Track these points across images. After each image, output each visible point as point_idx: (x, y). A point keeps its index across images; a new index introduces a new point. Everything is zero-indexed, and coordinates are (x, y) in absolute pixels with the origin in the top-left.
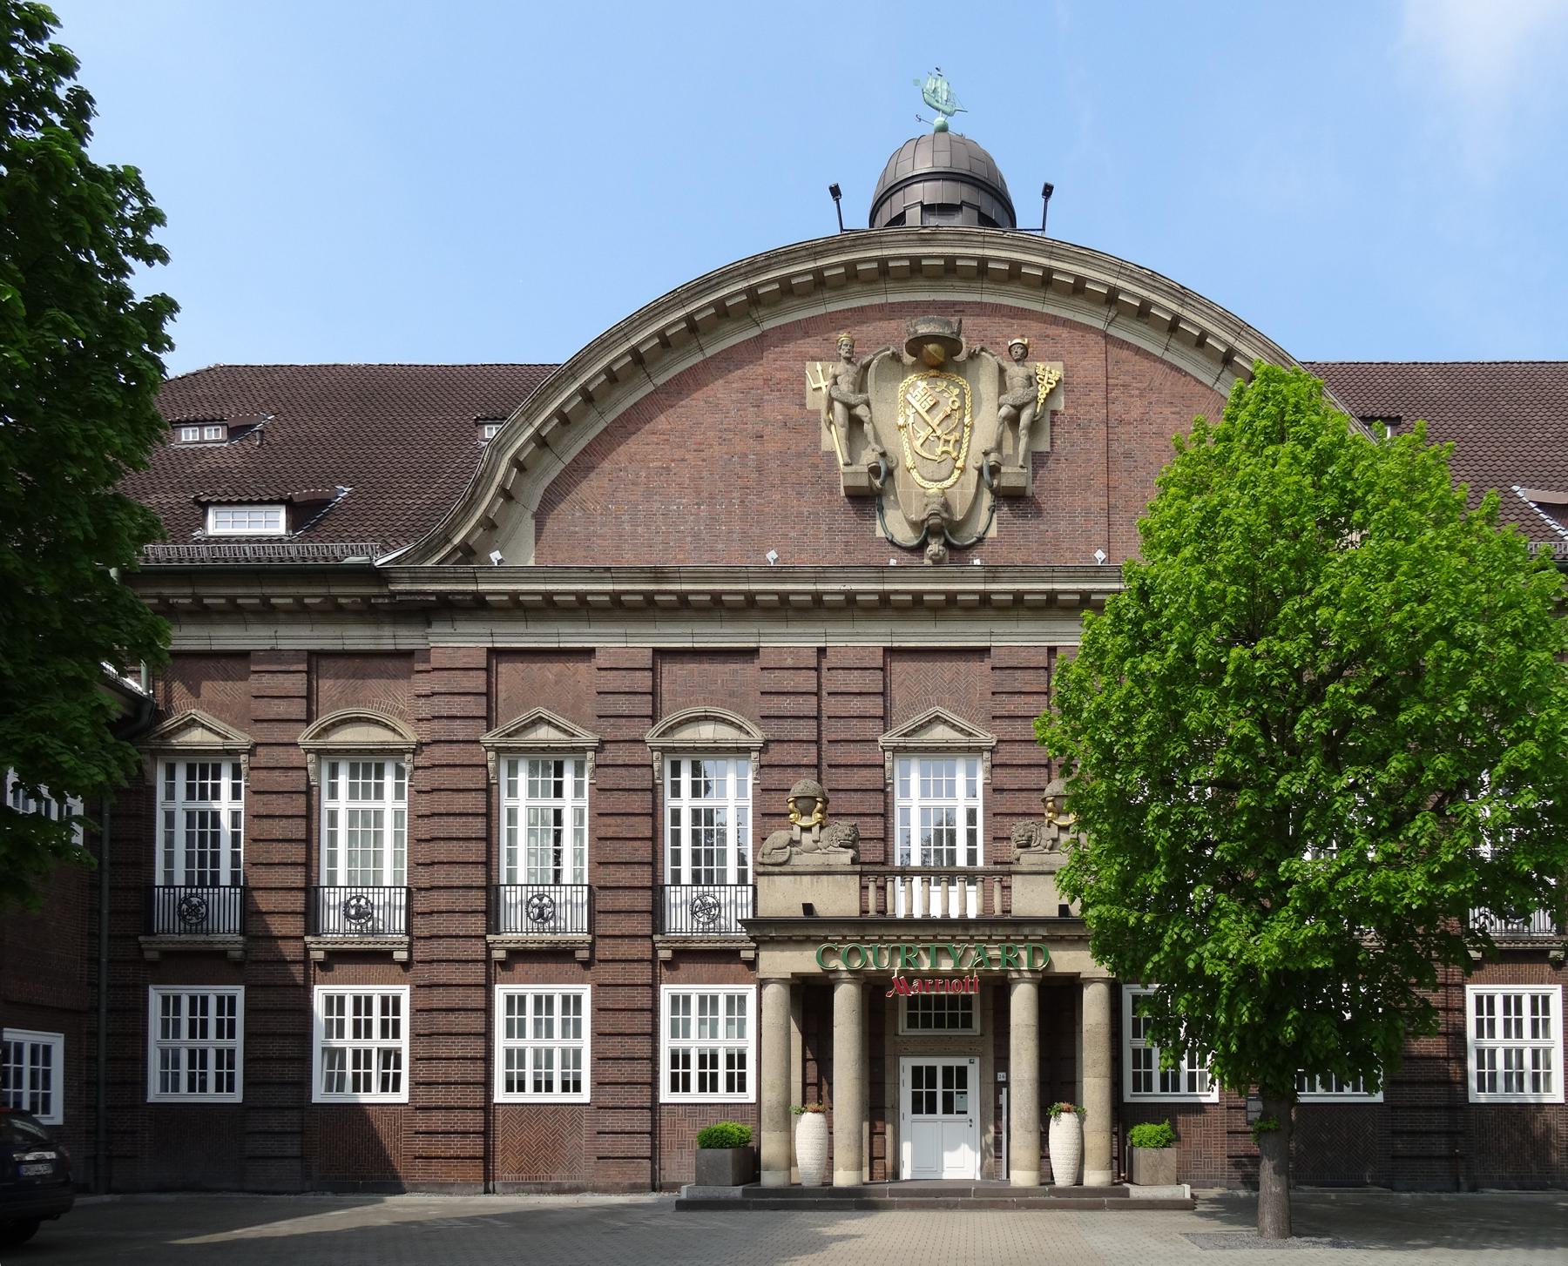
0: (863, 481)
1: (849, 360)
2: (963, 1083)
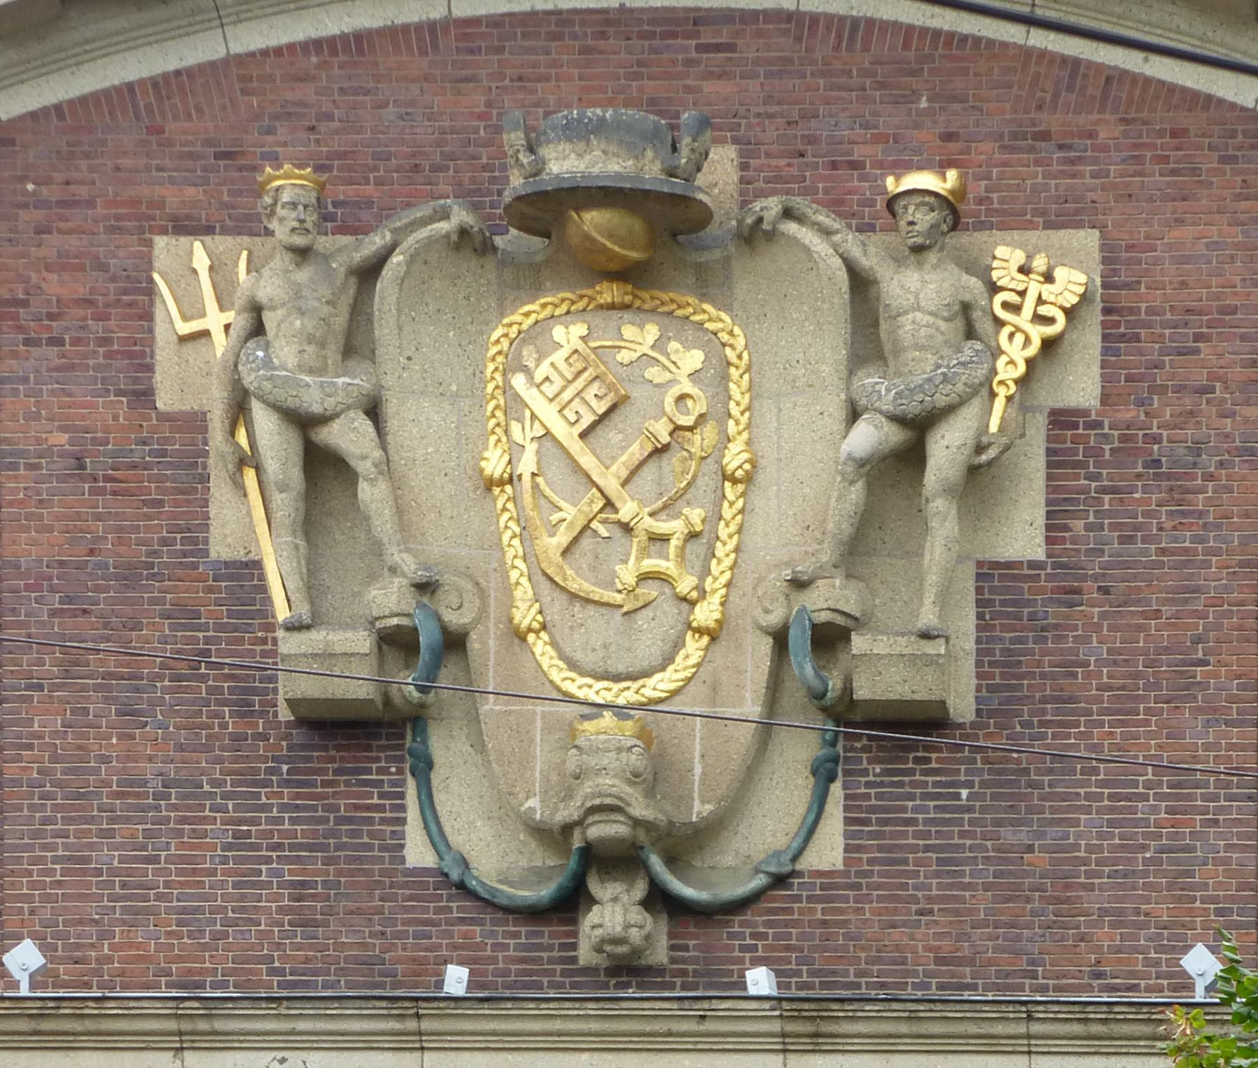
0: (356, 686)
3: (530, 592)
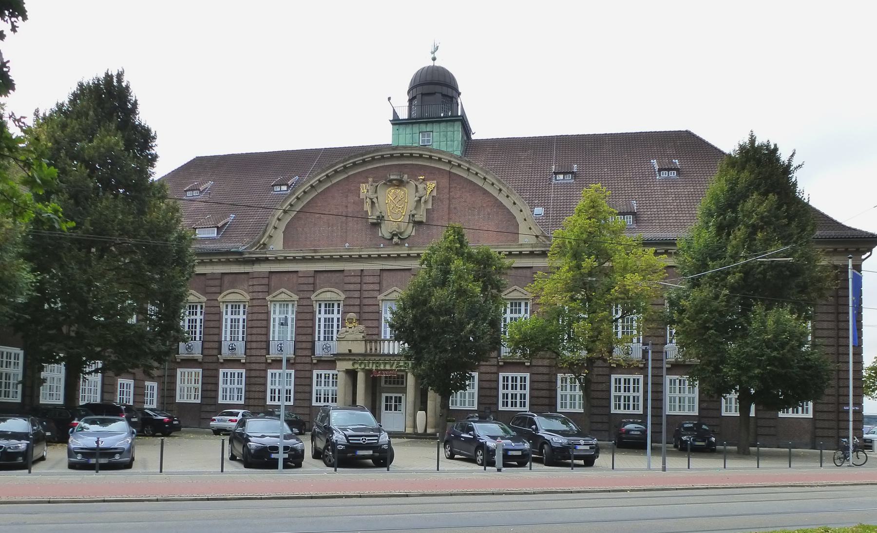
2: (400, 402)
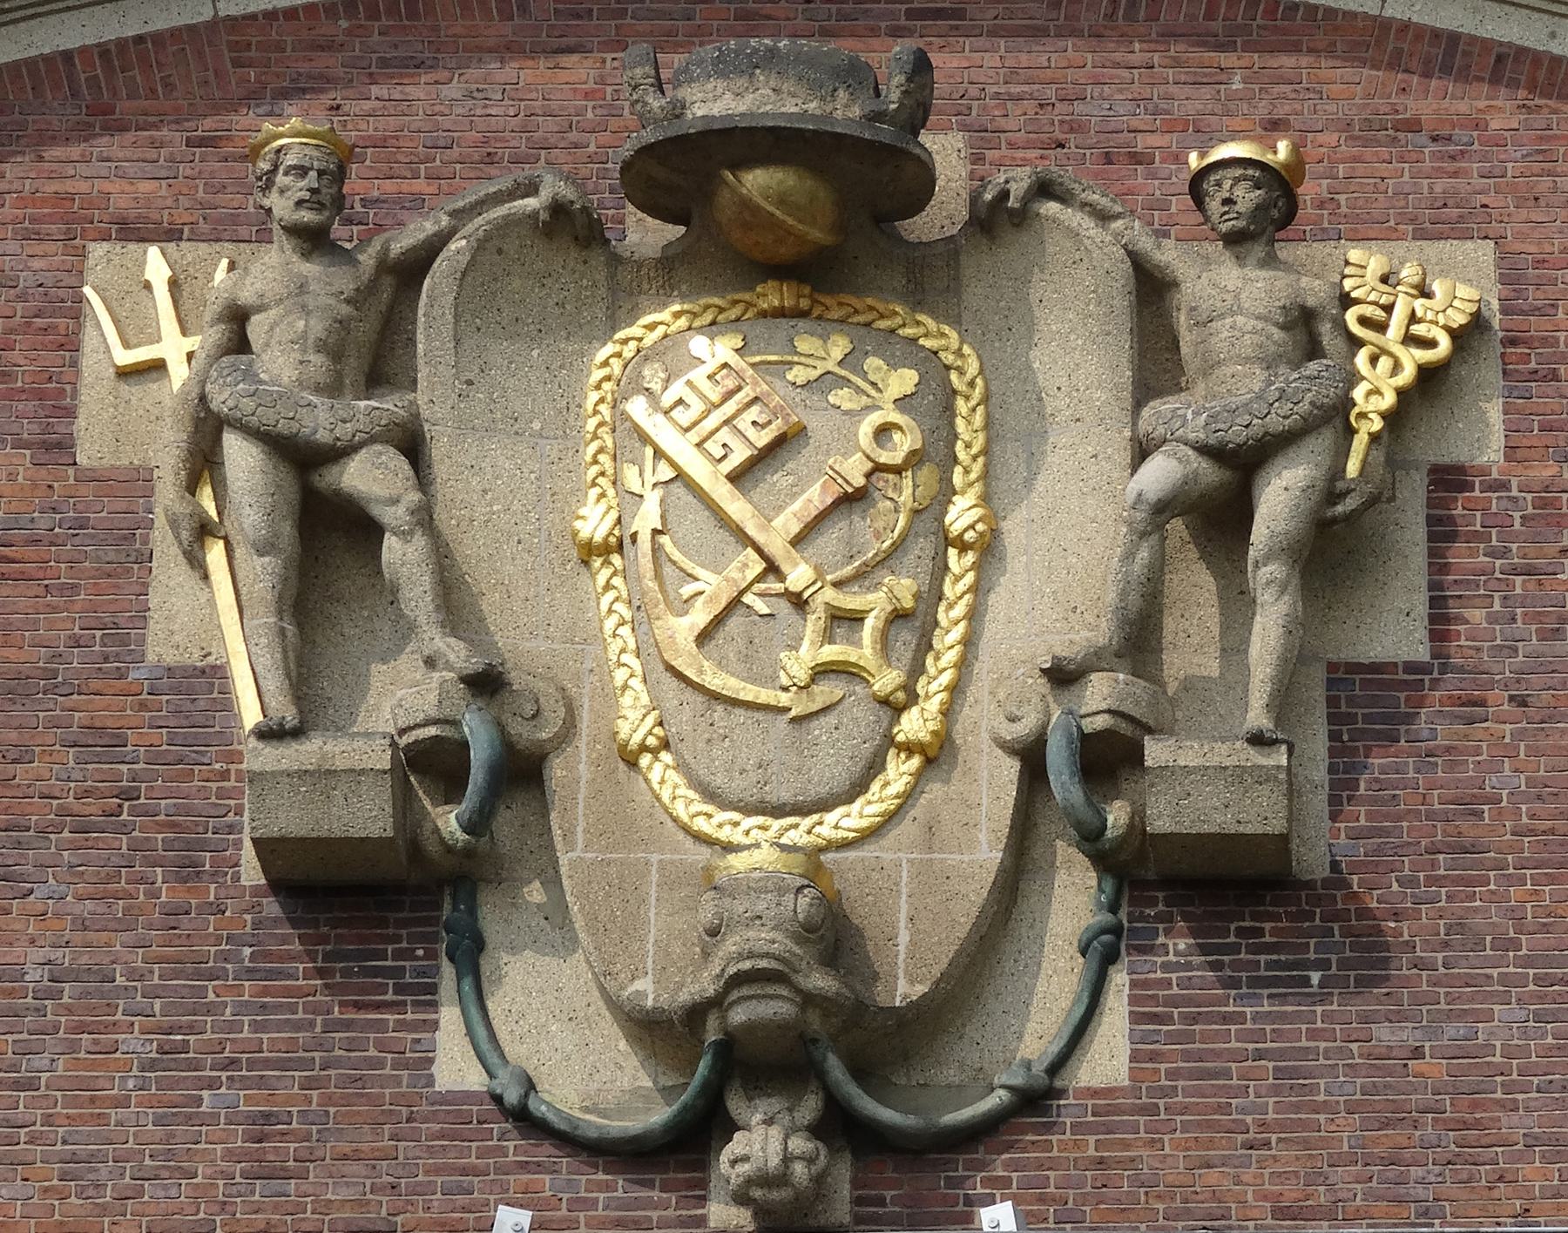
0: (368, 816)
1: (313, 240)
3: (645, 699)
